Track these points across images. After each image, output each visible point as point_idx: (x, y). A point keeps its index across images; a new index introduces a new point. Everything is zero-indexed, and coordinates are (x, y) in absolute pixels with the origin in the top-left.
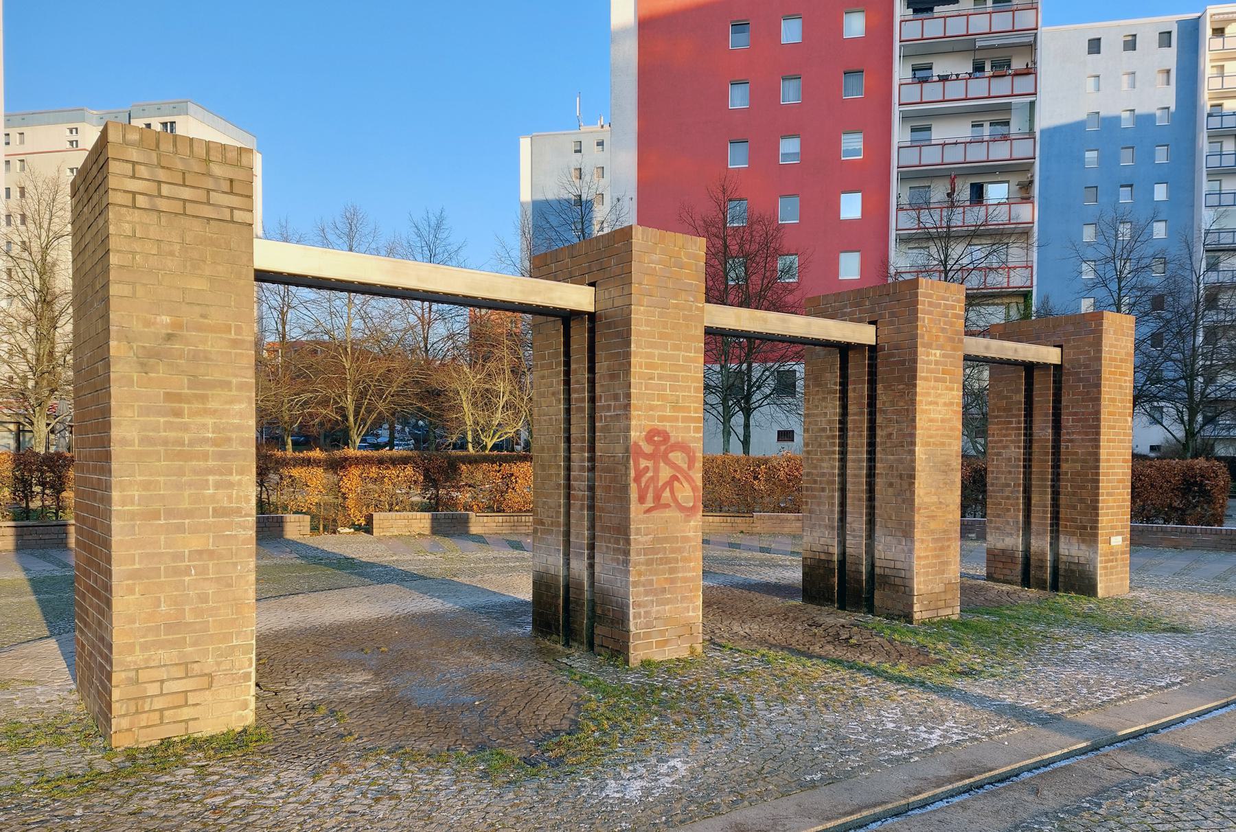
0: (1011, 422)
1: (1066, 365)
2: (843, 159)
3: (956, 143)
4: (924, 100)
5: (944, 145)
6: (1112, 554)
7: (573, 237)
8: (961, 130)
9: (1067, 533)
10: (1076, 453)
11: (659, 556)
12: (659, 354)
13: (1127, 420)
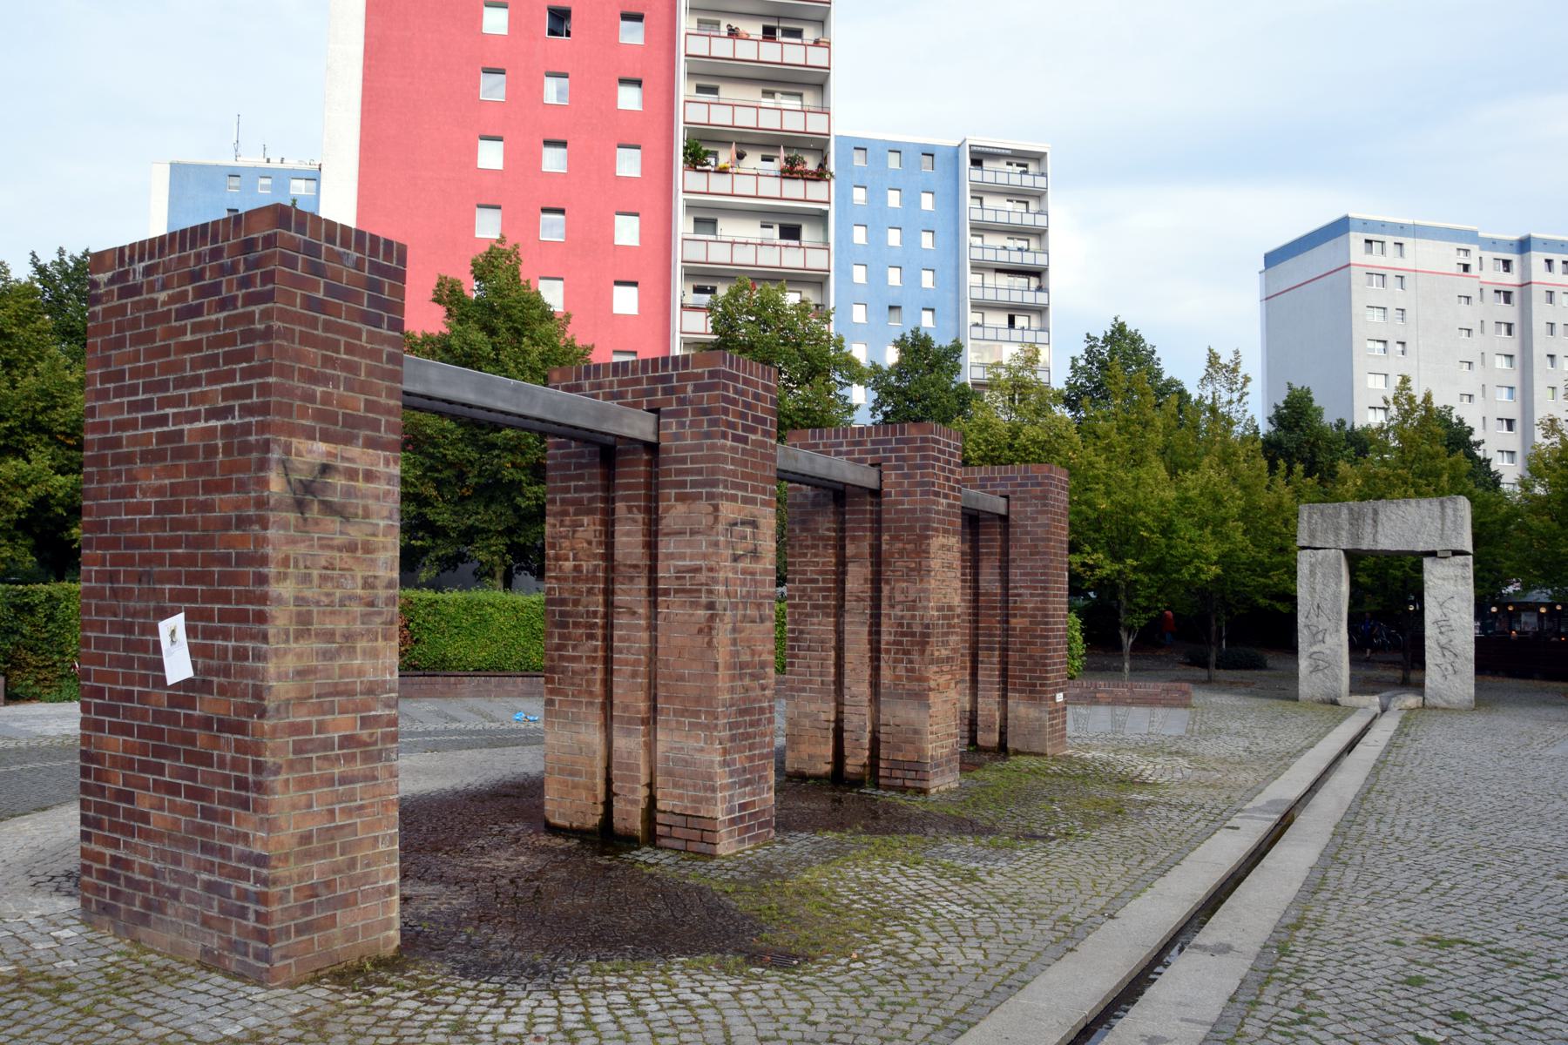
1: (1012, 516)
3: (746, 243)
5: (733, 243)
7: (1301, 542)
8: (750, 230)
9: (1015, 690)
10: (1025, 609)
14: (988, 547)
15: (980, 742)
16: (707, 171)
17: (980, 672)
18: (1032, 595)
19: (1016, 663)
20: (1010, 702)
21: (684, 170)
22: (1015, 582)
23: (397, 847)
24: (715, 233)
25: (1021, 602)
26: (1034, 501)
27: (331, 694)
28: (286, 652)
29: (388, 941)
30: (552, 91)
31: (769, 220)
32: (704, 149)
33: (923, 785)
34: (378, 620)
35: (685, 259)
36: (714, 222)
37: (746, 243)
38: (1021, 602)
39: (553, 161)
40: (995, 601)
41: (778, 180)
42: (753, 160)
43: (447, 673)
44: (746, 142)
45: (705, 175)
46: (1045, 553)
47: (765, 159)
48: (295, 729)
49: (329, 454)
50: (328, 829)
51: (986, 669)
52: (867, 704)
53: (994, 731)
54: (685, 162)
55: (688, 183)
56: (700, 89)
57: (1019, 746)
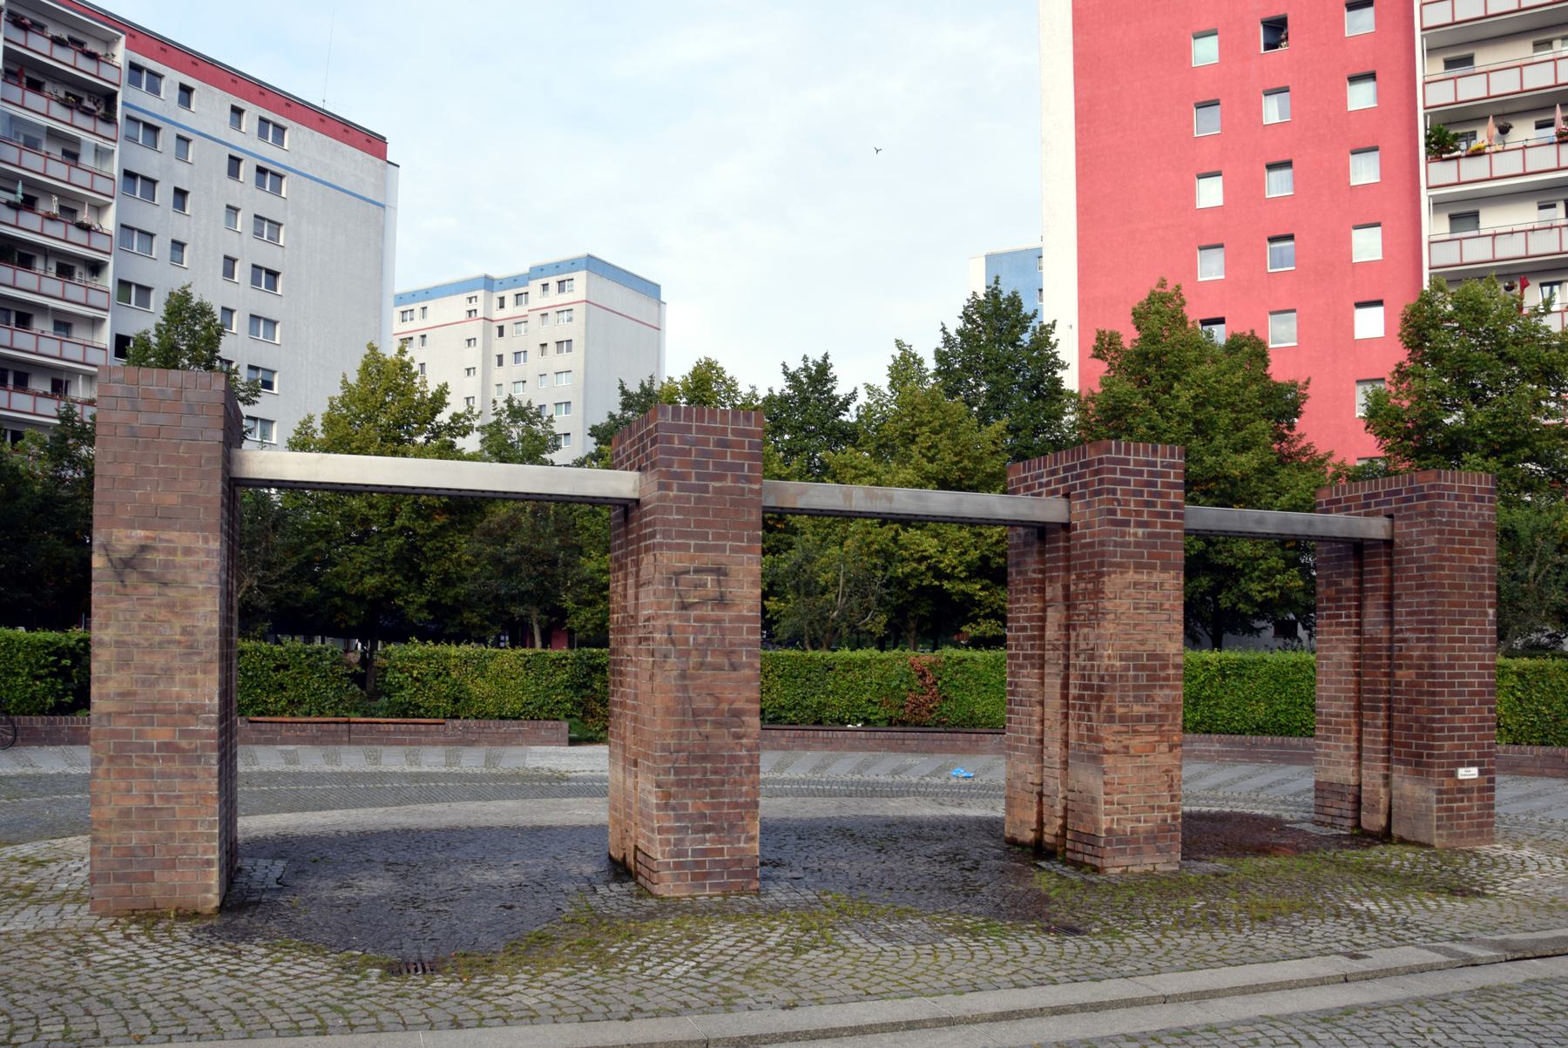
0: (1340, 616)
1: (1397, 540)
2: (1200, 279)
3: (1551, 228)
4: (1495, 175)
5: (1494, 236)
6: (1461, 791)
8: (1526, 215)
9: (1400, 762)
10: (1411, 657)
11: (696, 777)
12: (696, 545)
13: (1486, 614)
14: (1372, 581)
15: (1364, 825)
16: (1457, 158)
17: (1365, 737)
18: (1418, 640)
19: (1401, 727)
20: (1395, 776)
21: (1427, 162)
22: (1400, 623)
23: (217, 831)
24: (1477, 227)
25: (1408, 649)
26: (1420, 519)
27: (149, 711)
28: (107, 680)
29: (206, 901)
30: (1273, 111)
31: (1546, 199)
32: (1452, 132)
33: (1097, 862)
34: (197, 659)
35: (1433, 264)
36: (1476, 215)
37: (1512, 233)
38: (1408, 649)
39: (1278, 185)
40: (1379, 649)
41: (1553, 148)
42: (1524, 131)
43: (978, 730)
44: (1505, 113)
45: (1454, 164)
46: (1432, 585)
47: (1539, 126)
48: (114, 734)
49: (147, 538)
50: (147, 809)
51: (1370, 734)
52: (1058, 766)
53: (1377, 811)
54: (1428, 153)
55: (1437, 175)
56: (1449, 64)
57: (1404, 834)
